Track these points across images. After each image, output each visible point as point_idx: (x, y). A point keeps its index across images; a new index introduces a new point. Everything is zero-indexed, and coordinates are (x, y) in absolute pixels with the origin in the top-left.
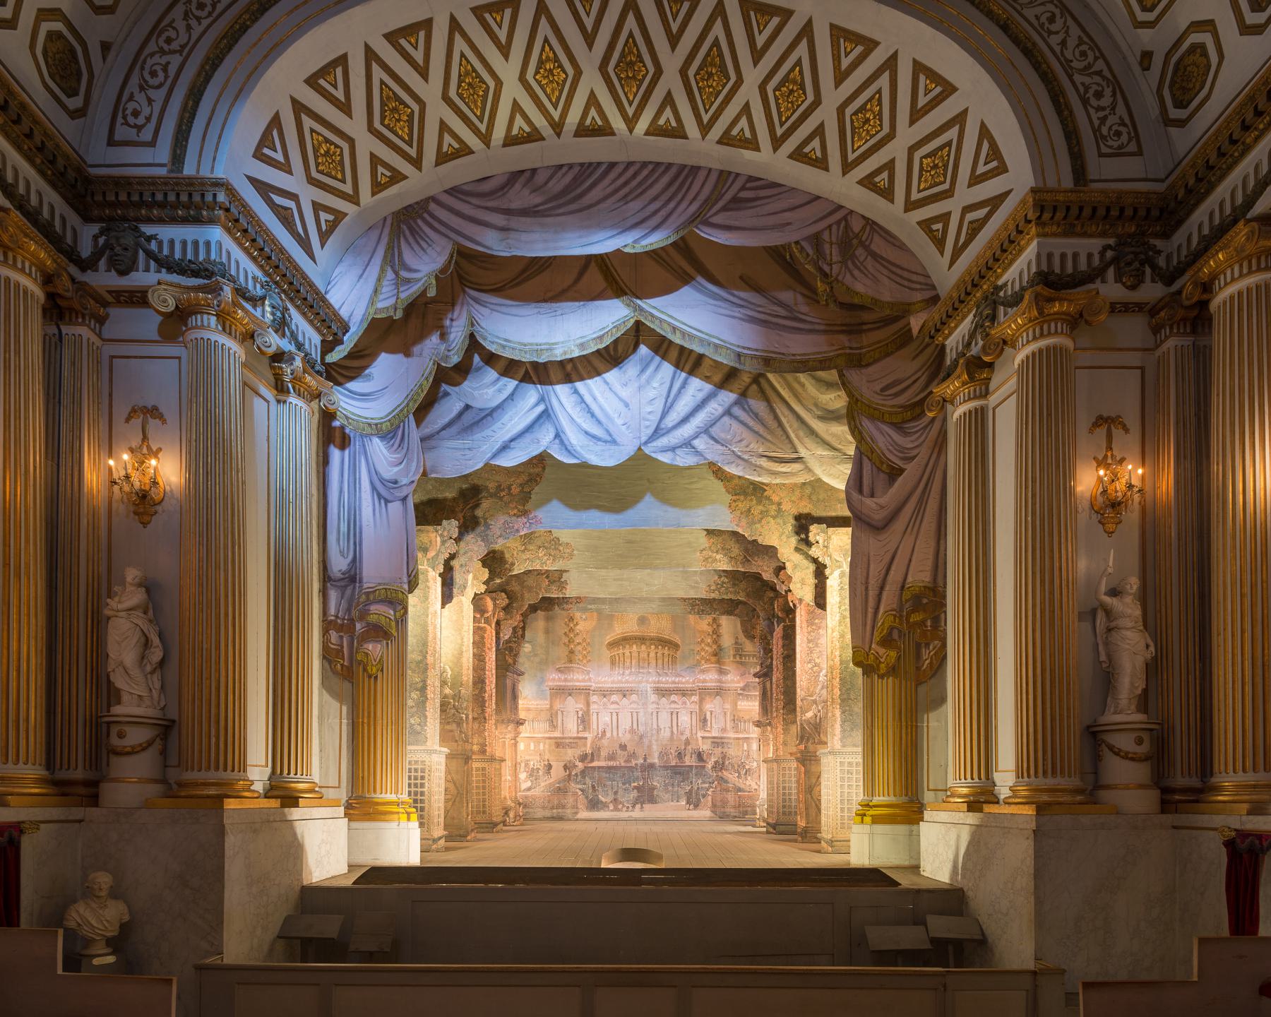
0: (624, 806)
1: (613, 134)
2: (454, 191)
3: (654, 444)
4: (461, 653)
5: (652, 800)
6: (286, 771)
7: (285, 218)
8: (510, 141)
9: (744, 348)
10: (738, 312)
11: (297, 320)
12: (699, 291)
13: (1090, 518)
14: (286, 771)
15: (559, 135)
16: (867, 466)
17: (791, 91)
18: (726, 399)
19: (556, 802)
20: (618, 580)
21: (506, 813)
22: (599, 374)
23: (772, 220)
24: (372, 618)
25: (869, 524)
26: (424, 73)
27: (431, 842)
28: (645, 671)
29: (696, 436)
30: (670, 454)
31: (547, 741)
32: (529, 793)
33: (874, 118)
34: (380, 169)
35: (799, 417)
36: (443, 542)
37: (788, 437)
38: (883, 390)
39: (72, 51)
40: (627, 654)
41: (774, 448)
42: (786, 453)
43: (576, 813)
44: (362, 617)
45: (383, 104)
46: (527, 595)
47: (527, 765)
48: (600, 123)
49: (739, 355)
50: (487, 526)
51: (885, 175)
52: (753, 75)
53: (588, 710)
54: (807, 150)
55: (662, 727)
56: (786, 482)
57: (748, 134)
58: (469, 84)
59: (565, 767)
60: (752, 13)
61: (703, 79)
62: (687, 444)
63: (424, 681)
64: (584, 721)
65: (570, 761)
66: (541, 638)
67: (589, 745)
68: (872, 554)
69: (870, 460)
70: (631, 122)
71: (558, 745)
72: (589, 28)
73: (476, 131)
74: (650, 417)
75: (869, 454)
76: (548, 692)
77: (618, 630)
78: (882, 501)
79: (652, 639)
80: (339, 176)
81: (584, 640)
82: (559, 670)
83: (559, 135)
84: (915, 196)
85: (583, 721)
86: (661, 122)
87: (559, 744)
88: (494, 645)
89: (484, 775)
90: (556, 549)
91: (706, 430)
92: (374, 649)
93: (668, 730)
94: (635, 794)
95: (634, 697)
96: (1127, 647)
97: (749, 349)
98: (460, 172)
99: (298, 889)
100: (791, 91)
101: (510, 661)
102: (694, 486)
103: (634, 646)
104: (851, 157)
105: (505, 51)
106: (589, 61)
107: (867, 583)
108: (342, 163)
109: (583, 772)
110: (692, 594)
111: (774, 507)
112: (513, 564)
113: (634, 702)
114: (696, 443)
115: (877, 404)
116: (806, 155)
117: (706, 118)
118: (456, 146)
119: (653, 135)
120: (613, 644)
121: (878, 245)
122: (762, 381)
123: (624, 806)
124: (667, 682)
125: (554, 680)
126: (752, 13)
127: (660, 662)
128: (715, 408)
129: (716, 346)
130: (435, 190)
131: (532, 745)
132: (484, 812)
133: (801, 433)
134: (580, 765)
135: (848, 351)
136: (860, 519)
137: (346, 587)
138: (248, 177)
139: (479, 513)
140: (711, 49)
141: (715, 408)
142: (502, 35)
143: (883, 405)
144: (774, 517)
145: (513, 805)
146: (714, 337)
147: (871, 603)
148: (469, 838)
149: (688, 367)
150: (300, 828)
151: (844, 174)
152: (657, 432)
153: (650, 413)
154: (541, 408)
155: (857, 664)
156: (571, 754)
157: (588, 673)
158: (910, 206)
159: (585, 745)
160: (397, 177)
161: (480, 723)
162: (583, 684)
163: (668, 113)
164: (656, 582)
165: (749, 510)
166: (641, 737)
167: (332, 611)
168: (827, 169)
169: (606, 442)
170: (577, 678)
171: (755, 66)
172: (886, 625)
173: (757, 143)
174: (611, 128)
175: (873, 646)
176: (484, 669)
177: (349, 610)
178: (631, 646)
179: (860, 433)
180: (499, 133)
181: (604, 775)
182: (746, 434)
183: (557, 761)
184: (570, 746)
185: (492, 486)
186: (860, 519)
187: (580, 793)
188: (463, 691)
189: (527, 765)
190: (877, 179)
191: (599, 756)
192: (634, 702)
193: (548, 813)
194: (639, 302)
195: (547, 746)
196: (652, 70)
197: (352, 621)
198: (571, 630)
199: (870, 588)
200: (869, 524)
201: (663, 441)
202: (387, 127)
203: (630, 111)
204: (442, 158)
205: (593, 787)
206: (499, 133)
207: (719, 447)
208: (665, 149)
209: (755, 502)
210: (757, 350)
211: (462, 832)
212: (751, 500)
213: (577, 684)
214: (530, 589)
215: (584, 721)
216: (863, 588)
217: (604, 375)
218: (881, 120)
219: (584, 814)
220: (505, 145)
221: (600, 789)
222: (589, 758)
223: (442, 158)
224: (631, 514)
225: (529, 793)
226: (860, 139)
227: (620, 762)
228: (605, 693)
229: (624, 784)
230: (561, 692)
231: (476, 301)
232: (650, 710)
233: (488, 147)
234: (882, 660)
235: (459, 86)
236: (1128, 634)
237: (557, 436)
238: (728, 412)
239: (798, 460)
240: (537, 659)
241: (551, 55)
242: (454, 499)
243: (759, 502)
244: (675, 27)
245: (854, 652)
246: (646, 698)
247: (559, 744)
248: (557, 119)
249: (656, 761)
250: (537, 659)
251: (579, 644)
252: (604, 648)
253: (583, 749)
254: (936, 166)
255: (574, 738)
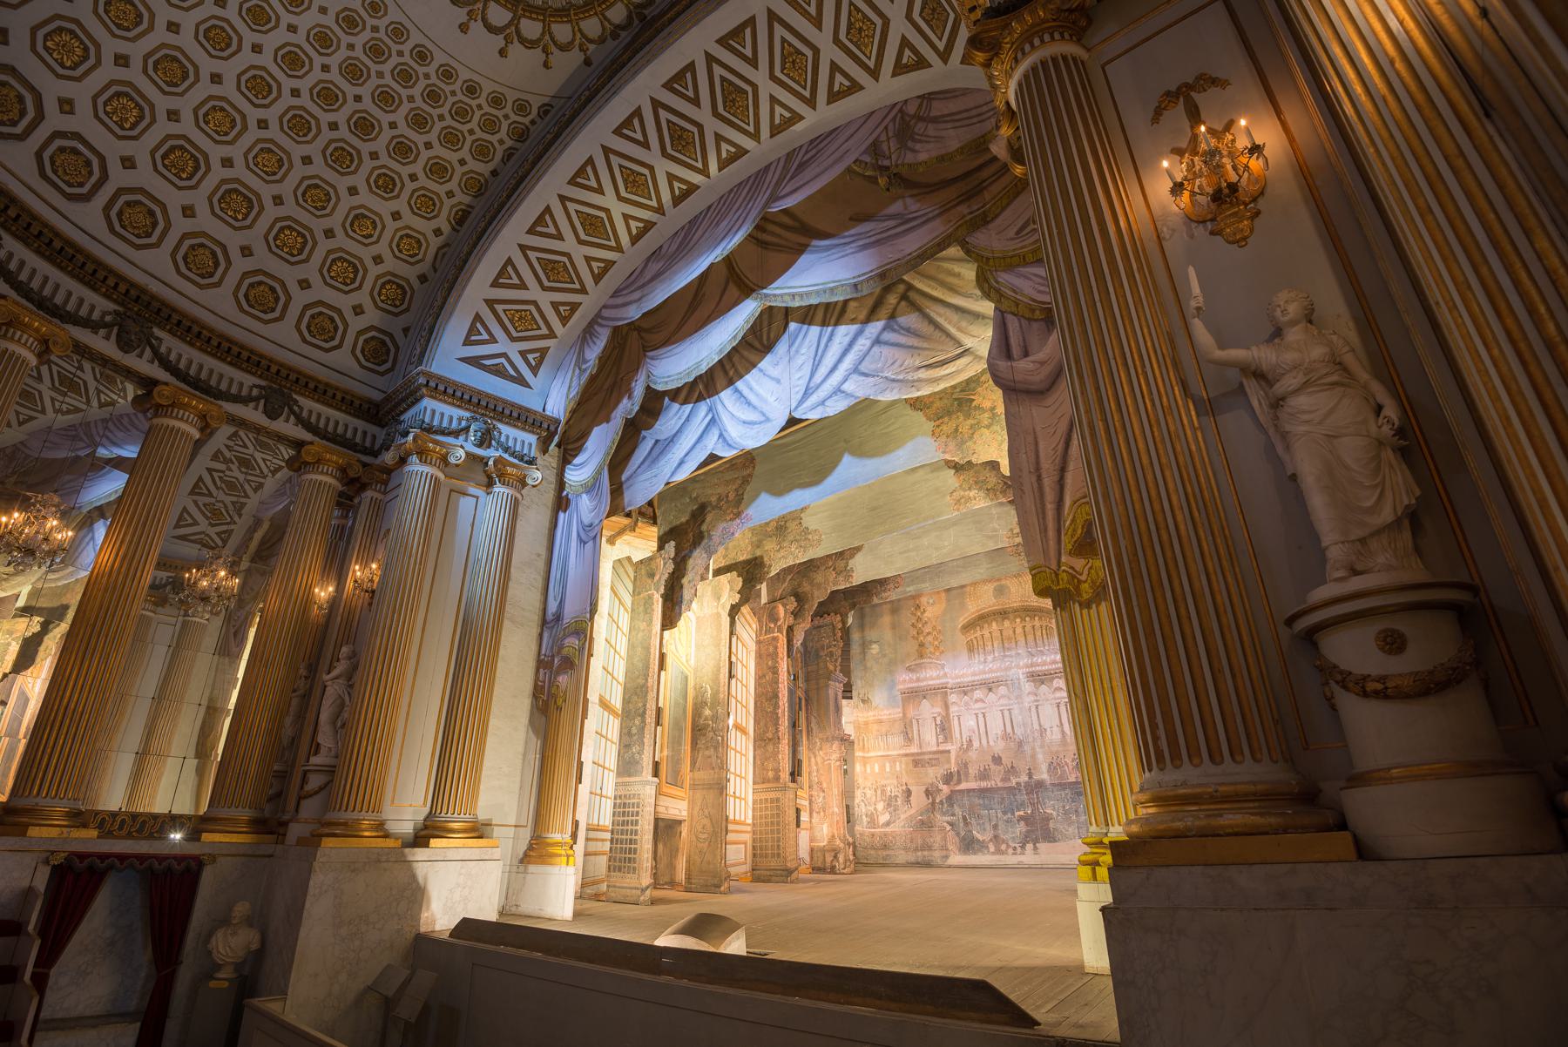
0: (1008, 846)
1: (698, 187)
2: (616, 294)
3: (805, 405)
4: (719, 670)
5: (1050, 837)
6: (439, 811)
7: (498, 372)
8: (635, 240)
9: (859, 276)
10: (849, 249)
11: (508, 432)
12: (816, 252)
13: (1192, 236)
14: (439, 811)
15: (664, 214)
16: (1013, 324)
17: (794, 62)
18: (873, 331)
19: (920, 841)
20: (905, 552)
21: (835, 857)
22: (754, 366)
23: (830, 160)
24: (565, 652)
25: (1028, 392)
26: (560, 237)
27: (639, 892)
28: (1013, 653)
29: (845, 380)
30: (820, 409)
31: (904, 759)
32: (887, 829)
33: (863, 23)
34: (561, 308)
35: (958, 309)
36: (665, 564)
37: (948, 335)
38: (1018, 233)
39: (383, 343)
40: (987, 635)
41: (933, 353)
42: (948, 352)
43: (947, 857)
44: (559, 653)
45: (544, 270)
46: (816, 593)
47: (883, 792)
48: (685, 187)
49: (855, 285)
50: (710, 537)
51: (907, 52)
52: (760, 76)
53: (948, 714)
54: (836, 88)
55: (1047, 726)
56: (953, 383)
57: (787, 115)
58: (590, 224)
59: (928, 793)
60: (731, 42)
61: (731, 107)
62: (838, 390)
63: (645, 705)
64: (944, 729)
65: (932, 784)
66: (888, 635)
67: (953, 761)
68: (1038, 429)
69: (1015, 315)
70: (704, 172)
71: (916, 763)
72: (642, 139)
73: (610, 248)
74: (800, 382)
75: (1014, 309)
76: (900, 697)
77: (972, 608)
78: (1040, 356)
79: (1016, 611)
80: (535, 327)
81: (934, 628)
82: (909, 669)
83: (664, 214)
84: (941, 45)
85: (943, 730)
86: (724, 155)
87: (918, 762)
88: (785, 653)
89: (778, 808)
90: (806, 539)
91: (856, 370)
92: (563, 680)
93: (1056, 730)
94: (1021, 828)
95: (1002, 690)
96: (1303, 428)
97: (863, 274)
98: (613, 280)
99: (410, 936)
100: (794, 62)
101: (831, 668)
102: (891, 429)
103: (994, 624)
104: (871, 64)
105: (600, 191)
106: (653, 157)
107: (1038, 468)
108: (533, 318)
109: (949, 798)
110: (992, 546)
111: (986, 415)
112: (770, 566)
113: (1002, 696)
114: (846, 387)
115: (1014, 250)
116: (839, 92)
117: (751, 129)
118: (603, 265)
119: (724, 168)
120: (968, 627)
121: (938, 108)
122: (912, 295)
123: (1008, 846)
124: (1044, 663)
125: (904, 681)
126: (731, 42)
127: (1031, 638)
128: (863, 343)
129: (832, 290)
130: (605, 300)
131: (888, 765)
132: (779, 855)
133: (964, 324)
134: (945, 789)
135: (968, 218)
136: (1014, 390)
137: (553, 627)
138: (459, 359)
139: (704, 528)
140: (722, 85)
141: (863, 343)
142: (593, 184)
143: (1022, 248)
144: (988, 427)
145: (842, 845)
146: (829, 283)
147: (1050, 496)
148: (722, 888)
149: (833, 321)
150: (421, 870)
151: (877, 80)
152: (807, 393)
153: (799, 379)
154: (710, 416)
155: (1041, 592)
156: (933, 774)
157: (943, 666)
158: (945, 56)
159: (949, 761)
160: (574, 307)
161: (774, 744)
162: (938, 682)
163: (724, 146)
164: (946, 544)
165: (956, 430)
166: (1020, 744)
167: (543, 652)
168: (862, 88)
169: (760, 423)
170: (931, 676)
171: (757, 69)
172: (1080, 522)
173: (798, 114)
174: (694, 184)
175: (1063, 559)
176: (777, 682)
177: (552, 648)
178: (990, 625)
179: (998, 291)
180: (625, 240)
181: (977, 801)
182: (898, 353)
183: (917, 784)
184: (930, 763)
185: (714, 499)
186: (1014, 390)
187: (949, 828)
188: (720, 710)
189: (883, 792)
190: (905, 61)
191: (967, 774)
192: (1002, 696)
193: (911, 857)
194: (765, 291)
195: (903, 766)
196: (695, 130)
197: (553, 656)
198: (919, 619)
199: (1044, 475)
200: (1028, 392)
201: (813, 399)
202: (554, 281)
203: (700, 165)
204: (597, 278)
205: (964, 818)
206: (625, 240)
207: (871, 379)
208: (740, 170)
209: (962, 418)
210: (871, 271)
211: (716, 881)
212: (958, 417)
213: (931, 682)
214: (819, 586)
215: (944, 729)
216: (1034, 479)
217: (759, 365)
218: (870, 20)
219: (957, 859)
220: (633, 244)
221: (973, 822)
222: (955, 778)
223: (597, 278)
224: (832, 481)
225: (887, 829)
226: (866, 46)
227: (995, 782)
228: (965, 690)
229: (1005, 813)
230: (914, 695)
231: (652, 358)
232: (1027, 705)
233: (623, 252)
234: (1083, 578)
235: (584, 230)
236: (1302, 401)
237: (721, 435)
238: (877, 341)
239: (966, 352)
240: (886, 660)
241: (628, 171)
242: (687, 521)
243: (968, 416)
244: (691, 94)
245: (1034, 576)
246: (1020, 688)
247: (918, 762)
248: (656, 206)
249: (1045, 776)
250: (886, 660)
251: (929, 634)
252: (959, 634)
253: (946, 766)
254: (934, 10)
255: (935, 753)
